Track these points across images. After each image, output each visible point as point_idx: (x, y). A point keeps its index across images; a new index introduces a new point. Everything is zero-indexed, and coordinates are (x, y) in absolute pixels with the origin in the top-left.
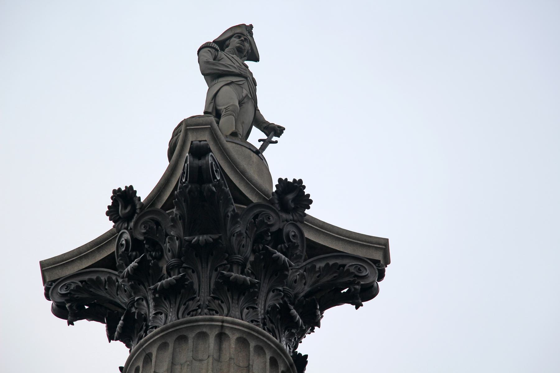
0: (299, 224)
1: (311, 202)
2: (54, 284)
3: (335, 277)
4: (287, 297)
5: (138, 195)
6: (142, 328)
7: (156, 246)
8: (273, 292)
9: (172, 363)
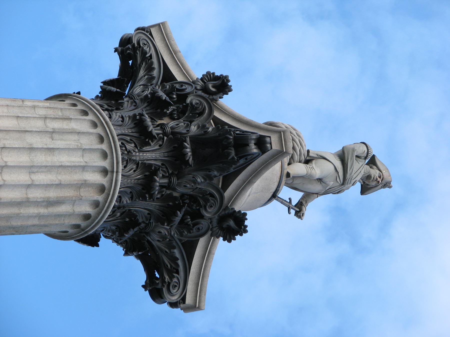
0: (210, 232)
1: (229, 241)
2: (148, 34)
3: (167, 266)
4: (146, 227)
5: (225, 96)
6: (111, 107)
7: (182, 113)
8: (148, 214)
9: (79, 132)
